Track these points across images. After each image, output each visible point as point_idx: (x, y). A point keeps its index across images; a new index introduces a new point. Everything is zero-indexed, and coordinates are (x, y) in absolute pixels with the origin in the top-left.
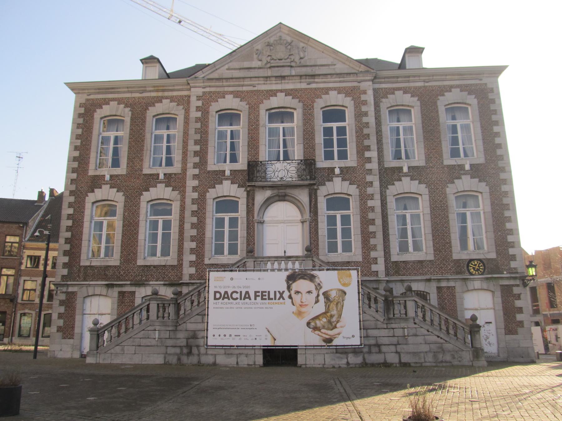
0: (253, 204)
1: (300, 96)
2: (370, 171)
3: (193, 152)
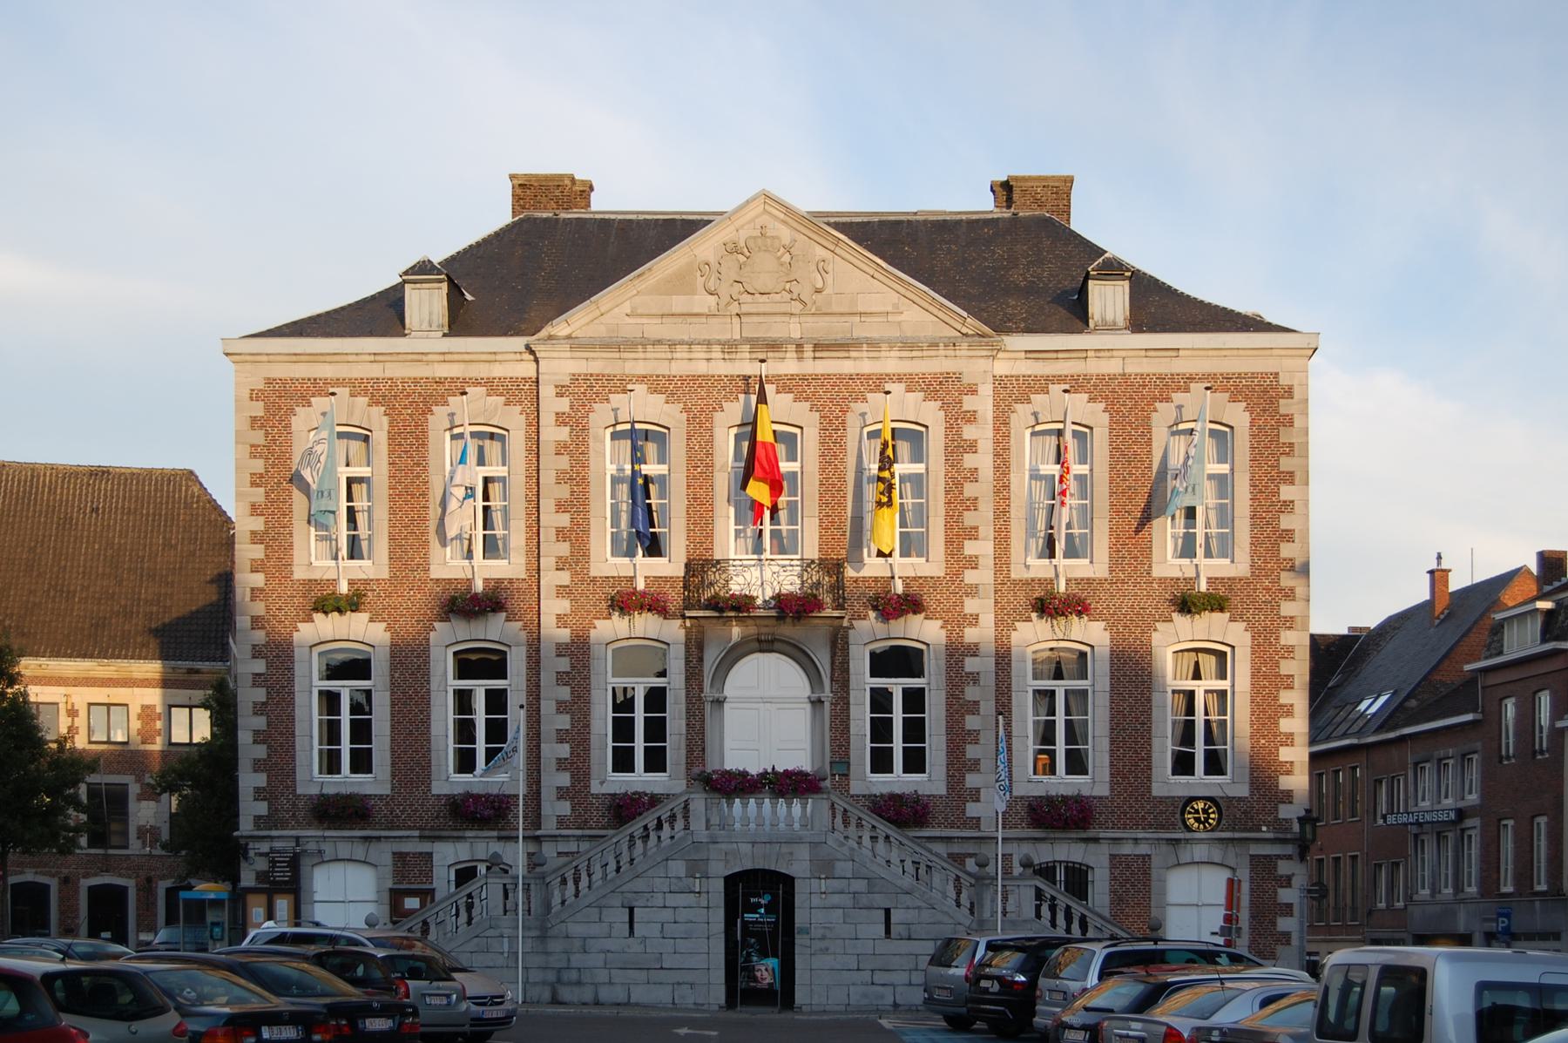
0: (701, 660)
2: (973, 591)
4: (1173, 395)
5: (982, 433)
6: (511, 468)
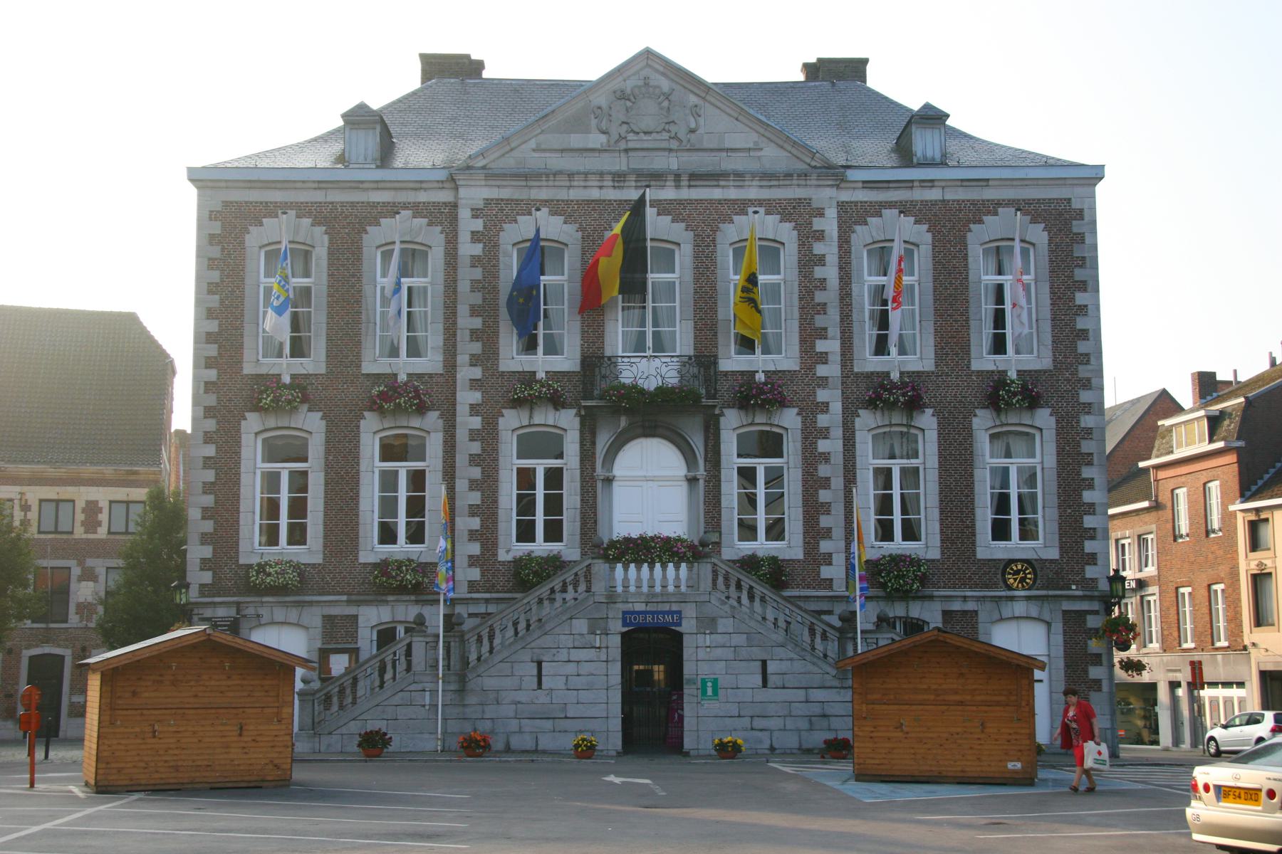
0: (594, 443)
1: (689, 216)
2: (824, 382)
3: (468, 332)
4: (985, 218)
5: (828, 250)
6: (429, 280)
